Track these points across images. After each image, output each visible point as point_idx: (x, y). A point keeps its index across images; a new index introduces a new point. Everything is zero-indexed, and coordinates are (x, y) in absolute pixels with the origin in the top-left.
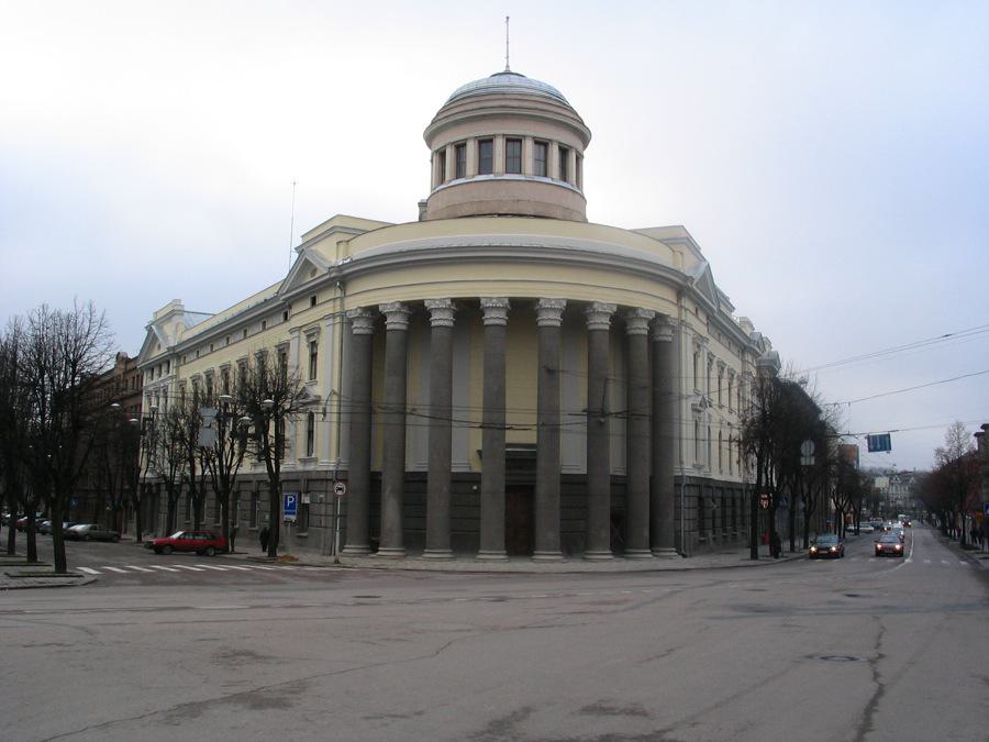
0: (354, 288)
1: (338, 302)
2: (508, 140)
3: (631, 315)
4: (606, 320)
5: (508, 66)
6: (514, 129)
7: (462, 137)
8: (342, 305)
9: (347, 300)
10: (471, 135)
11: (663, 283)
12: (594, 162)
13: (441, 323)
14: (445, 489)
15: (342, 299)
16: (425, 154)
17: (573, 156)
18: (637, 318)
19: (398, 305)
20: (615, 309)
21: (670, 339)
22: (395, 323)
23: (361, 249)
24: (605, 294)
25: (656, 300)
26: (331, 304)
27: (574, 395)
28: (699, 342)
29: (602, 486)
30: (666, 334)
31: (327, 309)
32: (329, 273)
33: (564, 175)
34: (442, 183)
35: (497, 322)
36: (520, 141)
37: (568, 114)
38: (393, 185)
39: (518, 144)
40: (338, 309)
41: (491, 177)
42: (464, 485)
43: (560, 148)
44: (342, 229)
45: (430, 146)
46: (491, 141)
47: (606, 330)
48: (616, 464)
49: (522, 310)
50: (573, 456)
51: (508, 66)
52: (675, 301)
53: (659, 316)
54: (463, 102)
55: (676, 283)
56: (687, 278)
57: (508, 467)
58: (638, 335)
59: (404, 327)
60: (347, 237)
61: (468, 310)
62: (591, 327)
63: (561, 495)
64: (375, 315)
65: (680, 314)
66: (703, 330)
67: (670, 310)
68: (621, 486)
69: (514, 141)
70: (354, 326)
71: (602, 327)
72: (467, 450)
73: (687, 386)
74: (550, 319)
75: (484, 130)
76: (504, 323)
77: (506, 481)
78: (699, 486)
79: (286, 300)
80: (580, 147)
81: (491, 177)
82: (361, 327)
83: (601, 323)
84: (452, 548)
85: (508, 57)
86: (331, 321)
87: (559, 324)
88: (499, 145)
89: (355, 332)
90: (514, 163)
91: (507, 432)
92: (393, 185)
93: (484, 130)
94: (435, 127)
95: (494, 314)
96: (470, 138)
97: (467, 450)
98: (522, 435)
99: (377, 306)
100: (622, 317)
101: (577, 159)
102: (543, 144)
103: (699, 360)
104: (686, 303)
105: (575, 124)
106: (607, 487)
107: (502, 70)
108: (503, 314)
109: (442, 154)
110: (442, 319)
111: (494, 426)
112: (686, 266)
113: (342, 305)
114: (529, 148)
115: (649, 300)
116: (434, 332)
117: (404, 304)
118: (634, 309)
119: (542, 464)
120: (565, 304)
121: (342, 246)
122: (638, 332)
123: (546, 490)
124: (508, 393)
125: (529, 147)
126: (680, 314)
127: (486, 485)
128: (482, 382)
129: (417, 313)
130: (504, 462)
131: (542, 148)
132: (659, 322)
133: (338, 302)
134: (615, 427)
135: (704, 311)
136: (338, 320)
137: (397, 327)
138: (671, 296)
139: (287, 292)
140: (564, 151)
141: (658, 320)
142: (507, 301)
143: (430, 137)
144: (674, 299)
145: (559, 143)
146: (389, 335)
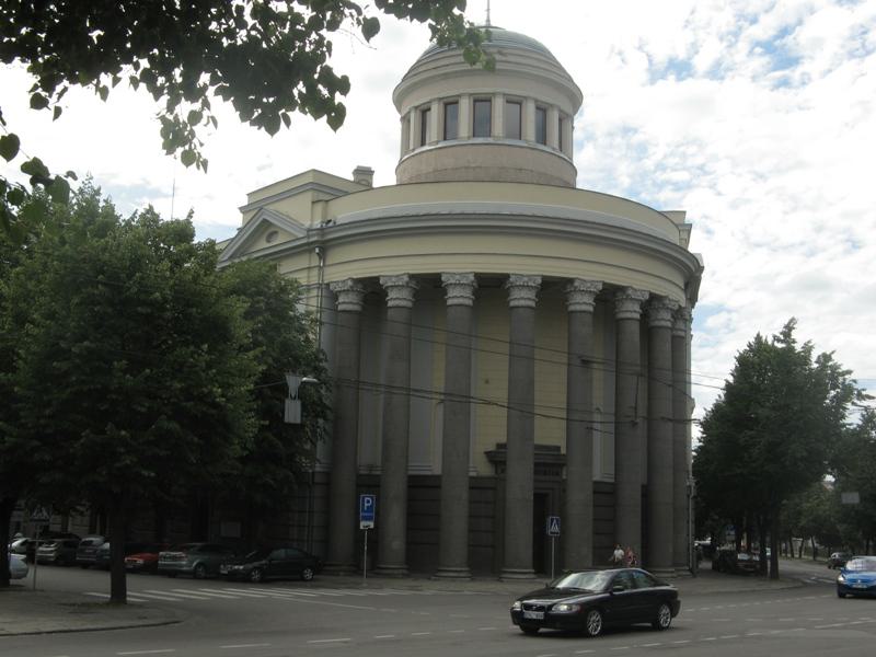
0: (335, 256)
2: (475, 101)
3: (620, 295)
4: (589, 299)
5: (488, 21)
6: (517, 89)
7: (550, 101)
9: (328, 271)
10: (532, 94)
11: (669, 264)
16: (394, 118)
17: (554, 117)
19: (406, 279)
20: (600, 287)
24: (589, 269)
25: (652, 280)
27: (551, 389)
30: (664, 319)
32: (308, 237)
33: (542, 137)
34: (423, 144)
35: (461, 301)
36: (490, 101)
37: (555, 70)
39: (488, 104)
41: (490, 140)
43: (538, 108)
46: (457, 103)
47: (590, 312)
49: (491, 287)
51: (488, 21)
53: (654, 298)
54: (437, 57)
57: (536, 473)
59: (410, 304)
60: (327, 197)
61: (429, 288)
62: (572, 308)
63: (595, 506)
69: (482, 101)
70: (341, 300)
71: (584, 308)
74: (582, 303)
77: (535, 488)
81: (490, 140)
83: (582, 303)
84: (469, 566)
85: (488, 10)
87: (591, 309)
88: (465, 107)
89: (340, 308)
90: (481, 125)
93: (448, 90)
94: (408, 83)
95: (524, 293)
96: (499, 93)
98: (550, 432)
99: (377, 278)
100: (609, 296)
101: (560, 120)
108: (468, 292)
109: (405, 119)
113: (321, 275)
117: (412, 277)
118: (622, 289)
120: (540, 281)
122: (628, 315)
123: (579, 500)
124: (537, 386)
129: (372, 291)
130: (532, 466)
131: (541, 113)
132: (655, 303)
133: (315, 272)
137: (350, 307)
140: (542, 110)
141: (652, 303)
142: (472, 278)
143: (399, 98)
145: (536, 101)
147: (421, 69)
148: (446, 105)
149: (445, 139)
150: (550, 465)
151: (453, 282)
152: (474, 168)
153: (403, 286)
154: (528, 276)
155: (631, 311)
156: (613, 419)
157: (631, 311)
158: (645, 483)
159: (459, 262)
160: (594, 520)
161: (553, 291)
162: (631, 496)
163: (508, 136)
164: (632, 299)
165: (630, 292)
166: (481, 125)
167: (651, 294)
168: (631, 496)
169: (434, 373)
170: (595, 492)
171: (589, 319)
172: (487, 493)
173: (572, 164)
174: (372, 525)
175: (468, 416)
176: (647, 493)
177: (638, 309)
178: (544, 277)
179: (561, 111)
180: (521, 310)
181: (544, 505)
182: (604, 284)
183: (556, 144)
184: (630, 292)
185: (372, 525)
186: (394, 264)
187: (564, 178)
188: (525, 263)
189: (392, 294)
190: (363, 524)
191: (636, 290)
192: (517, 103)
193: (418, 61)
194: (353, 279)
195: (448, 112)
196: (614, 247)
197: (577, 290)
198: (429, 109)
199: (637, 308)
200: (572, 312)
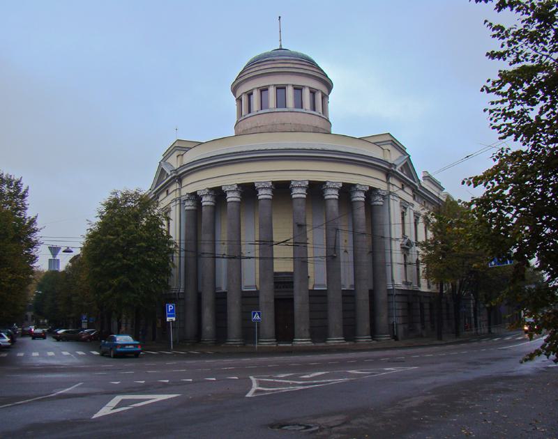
0: (186, 181)
1: (178, 191)
2: (277, 88)
3: (353, 189)
5: (281, 46)
8: (180, 193)
9: (182, 190)
12: (335, 100)
13: (233, 199)
14: (237, 302)
15: (180, 189)
17: (319, 96)
18: (356, 191)
21: (381, 203)
22: (207, 201)
23: (190, 157)
24: (334, 176)
26: (174, 193)
27: (316, 241)
28: (404, 206)
29: (335, 299)
30: (378, 201)
31: (173, 196)
35: (266, 197)
36: (285, 88)
38: (212, 117)
39: (299, 91)
40: (178, 196)
41: (267, 111)
42: (250, 300)
43: (311, 92)
44: (180, 147)
45: (235, 95)
46: (267, 90)
48: (347, 281)
49: (282, 189)
50: (317, 276)
51: (281, 46)
52: (385, 180)
55: (385, 168)
56: (391, 165)
58: (358, 201)
61: (248, 191)
64: (195, 197)
65: (389, 188)
66: (410, 199)
67: (381, 186)
68: (349, 296)
69: (281, 88)
70: (203, 200)
71: (333, 197)
72: (251, 276)
73: (396, 232)
75: (281, 80)
76: (270, 197)
78: (430, 297)
79: (155, 193)
80: (325, 90)
81: (302, 110)
82: (189, 205)
86: (174, 204)
87: (305, 196)
88: (272, 91)
89: (187, 208)
90: (281, 102)
91: (217, 259)
92: (212, 117)
95: (299, 191)
97: (251, 276)
98: (283, 265)
100: (346, 190)
101: (322, 98)
102: (299, 89)
103: (407, 218)
104: (392, 180)
105: (326, 79)
106: (339, 297)
107: (279, 48)
109: (239, 100)
110: (232, 197)
111: (267, 259)
112: (393, 157)
114: (290, 92)
115: (364, 179)
116: (229, 205)
117: (211, 189)
119: (297, 284)
120: (341, 186)
121: (180, 157)
122: (358, 199)
125: (290, 91)
126: (389, 188)
127: (262, 299)
128: (292, 231)
129: (219, 194)
130: (273, 284)
133: (178, 191)
134: (222, 249)
135: (408, 186)
136: (178, 202)
137: (208, 203)
138: (383, 177)
139: (155, 188)
140: (313, 92)
141: (371, 192)
143: (234, 90)
144: (384, 179)
145: (310, 88)
146: (203, 208)
147: (244, 74)
148: (261, 91)
149: (261, 109)
150: (283, 283)
151: (261, 186)
152: (260, 127)
153: (234, 191)
154: (264, 182)
155: (359, 197)
156: (217, 242)
157: (359, 197)
158: (371, 288)
159: (263, 175)
160: (343, 311)
161: (316, 190)
162: (363, 298)
163: (296, 107)
164: (359, 190)
165: (358, 187)
166: (281, 102)
167: (370, 187)
168: (363, 298)
169: (250, 234)
170: (343, 296)
171: (363, 204)
172: (284, 305)
173: (328, 120)
174: (174, 319)
175: (255, 259)
176: (372, 294)
177: (363, 196)
178: (343, 183)
179: (322, 93)
180: (332, 201)
181: (284, 305)
182: (309, 181)
183: (321, 112)
184: (358, 187)
185: (174, 319)
186: (229, 178)
187: (325, 129)
188: (300, 174)
189: (229, 195)
190: (168, 319)
191: (361, 185)
192: (299, 89)
193: (244, 69)
194: (208, 188)
195: (278, 94)
196: (368, 167)
197: (379, 195)
198: (252, 94)
199: (363, 195)
200: (355, 201)
